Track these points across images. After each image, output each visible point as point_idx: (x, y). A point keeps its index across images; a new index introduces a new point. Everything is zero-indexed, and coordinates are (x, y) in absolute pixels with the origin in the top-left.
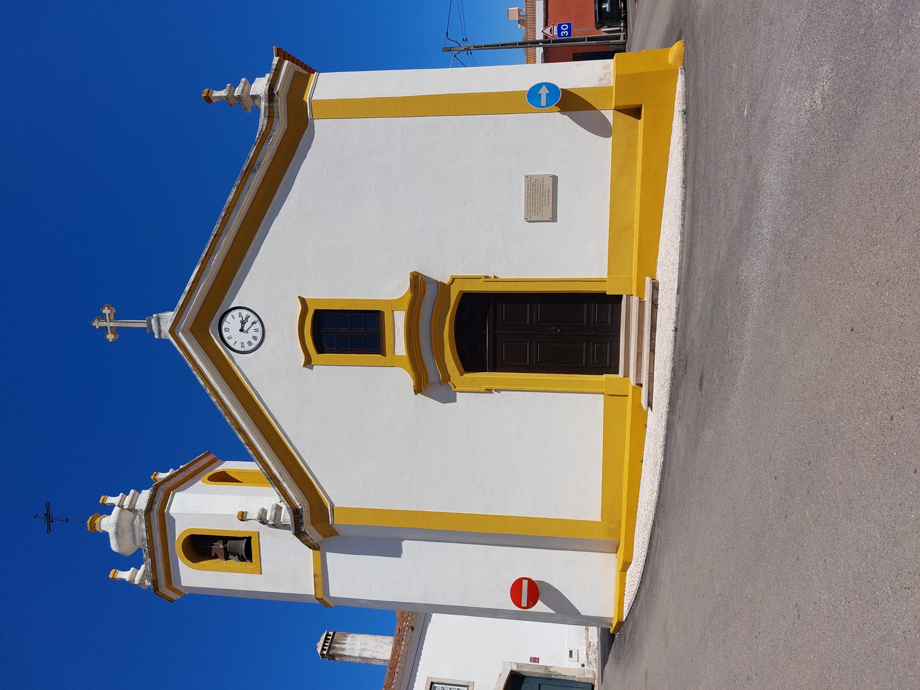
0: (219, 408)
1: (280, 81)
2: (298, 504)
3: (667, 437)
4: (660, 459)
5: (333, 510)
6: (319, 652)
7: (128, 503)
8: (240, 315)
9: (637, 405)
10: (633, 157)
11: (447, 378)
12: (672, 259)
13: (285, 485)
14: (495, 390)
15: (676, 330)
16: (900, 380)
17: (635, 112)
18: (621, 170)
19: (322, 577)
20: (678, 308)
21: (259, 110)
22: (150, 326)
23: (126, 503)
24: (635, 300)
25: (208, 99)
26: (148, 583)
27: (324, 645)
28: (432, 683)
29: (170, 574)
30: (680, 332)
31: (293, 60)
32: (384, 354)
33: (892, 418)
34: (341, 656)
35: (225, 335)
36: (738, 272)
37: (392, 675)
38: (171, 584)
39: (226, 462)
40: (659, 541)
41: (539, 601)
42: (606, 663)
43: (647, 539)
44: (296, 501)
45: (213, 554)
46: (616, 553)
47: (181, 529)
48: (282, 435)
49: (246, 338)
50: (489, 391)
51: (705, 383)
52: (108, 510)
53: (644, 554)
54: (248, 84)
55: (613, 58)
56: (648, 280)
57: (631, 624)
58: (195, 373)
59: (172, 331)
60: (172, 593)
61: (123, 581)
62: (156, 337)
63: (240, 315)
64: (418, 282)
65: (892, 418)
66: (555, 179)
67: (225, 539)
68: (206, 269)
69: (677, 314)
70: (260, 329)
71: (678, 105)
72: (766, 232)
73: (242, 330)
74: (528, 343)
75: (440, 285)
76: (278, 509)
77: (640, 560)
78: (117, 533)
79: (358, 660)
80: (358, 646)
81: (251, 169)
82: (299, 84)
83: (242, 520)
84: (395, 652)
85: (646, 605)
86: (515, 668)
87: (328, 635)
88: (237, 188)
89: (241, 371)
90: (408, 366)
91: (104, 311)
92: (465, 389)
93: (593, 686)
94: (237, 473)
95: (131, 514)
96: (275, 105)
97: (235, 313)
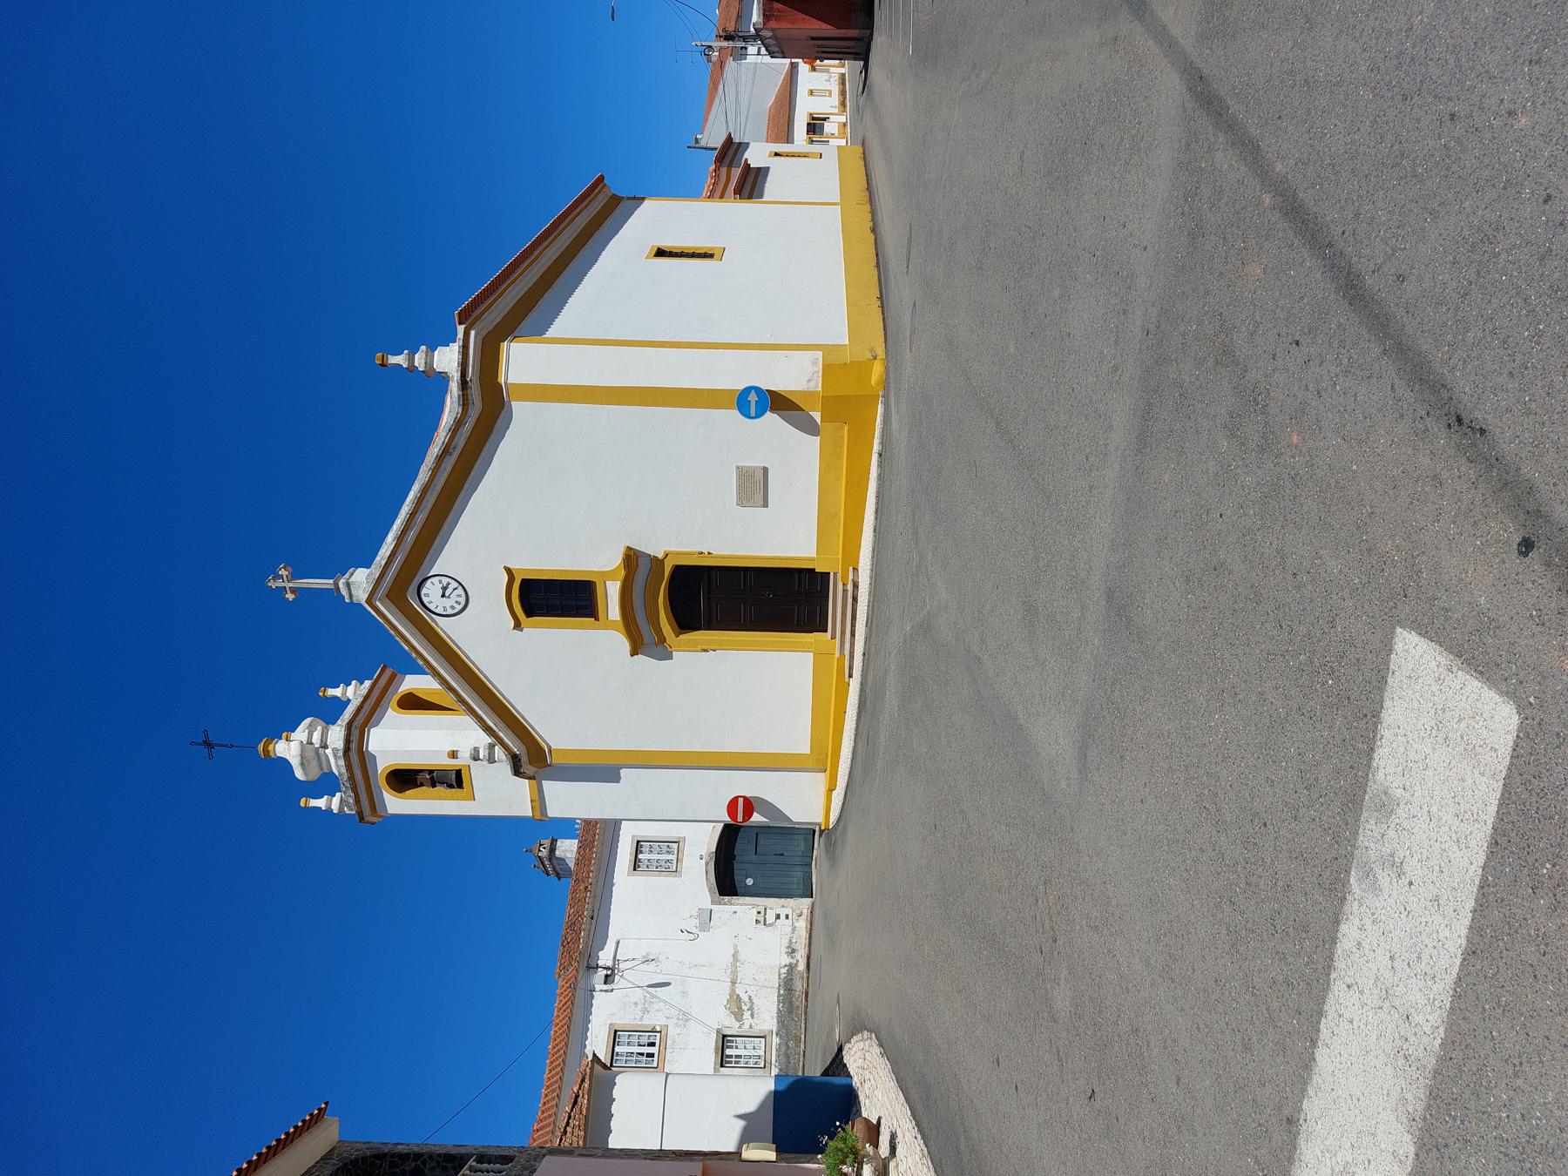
1: (471, 362)
2: (515, 750)
5: (550, 751)
8: (440, 582)
11: (662, 640)
13: (501, 734)
19: (539, 800)
22: (336, 584)
28: (638, 842)
29: (375, 804)
32: (597, 619)
35: (425, 600)
41: (755, 813)
47: (383, 765)
48: (501, 697)
49: (447, 603)
58: (397, 639)
63: (440, 582)
64: (632, 558)
66: (765, 470)
73: (443, 596)
78: (302, 764)
89: (445, 633)
90: (623, 630)
94: (426, 693)
96: (469, 392)
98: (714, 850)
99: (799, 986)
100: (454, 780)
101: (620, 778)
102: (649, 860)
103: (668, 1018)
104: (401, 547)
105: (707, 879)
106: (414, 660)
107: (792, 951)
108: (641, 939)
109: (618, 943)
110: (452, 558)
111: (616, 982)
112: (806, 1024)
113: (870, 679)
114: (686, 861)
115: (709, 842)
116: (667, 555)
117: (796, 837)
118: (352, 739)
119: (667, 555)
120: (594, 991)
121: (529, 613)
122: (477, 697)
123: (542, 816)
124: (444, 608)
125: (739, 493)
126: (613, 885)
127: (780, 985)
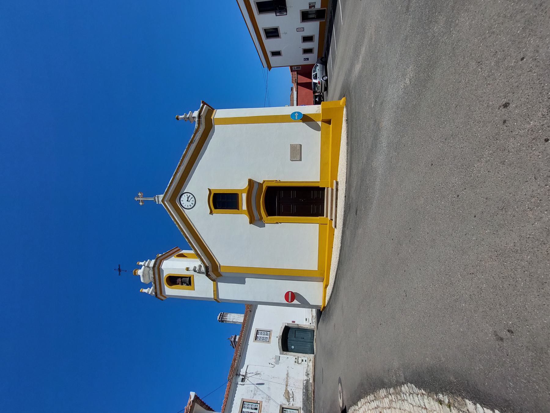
0: (179, 229)
2: (207, 264)
3: (342, 237)
4: (340, 245)
5: (220, 266)
6: (218, 320)
7: (147, 264)
8: (187, 195)
9: (331, 226)
10: (329, 134)
11: (261, 218)
12: (343, 172)
14: (279, 223)
15: (345, 197)
16: (462, 177)
17: (329, 122)
18: (324, 143)
19: (216, 291)
20: (346, 189)
21: (195, 122)
22: (155, 199)
23: (146, 265)
24: (330, 189)
25: (177, 119)
26: (154, 294)
27: (220, 317)
28: (257, 330)
30: (347, 197)
31: (207, 104)
32: (238, 209)
33: (458, 196)
34: (226, 321)
35: (182, 202)
36: (371, 165)
37: (243, 328)
38: (162, 294)
39: (183, 250)
40: (339, 275)
41: (295, 300)
42: (319, 322)
43: (335, 275)
44: (206, 263)
45: (177, 283)
46: (323, 282)
50: (277, 223)
51: (358, 212)
52: (140, 267)
53: (333, 281)
54: (192, 113)
55: (320, 104)
56: (334, 181)
57: (328, 307)
58: (170, 216)
59: (163, 201)
60: (162, 297)
61: (145, 293)
62: (157, 203)
63: (187, 195)
64: (251, 182)
65: (458, 196)
66: (301, 145)
67: (182, 278)
68: (175, 178)
69: (346, 191)
70: (194, 200)
71: (344, 118)
72: (384, 144)
73: (188, 201)
74: (291, 205)
75: (259, 184)
76: (200, 266)
77: (332, 283)
78: (143, 276)
79: (232, 322)
80: (232, 318)
81: (192, 142)
82: (210, 111)
83: (187, 270)
84: (245, 320)
85: (334, 300)
86: (287, 325)
87: (221, 314)
88: (187, 149)
91: (139, 194)
92: (268, 222)
93: (314, 331)
95: (148, 269)
97: (185, 195)
98: (281, 335)
99: (311, 389)
100: (187, 281)
101: (245, 282)
102: (260, 337)
103: (263, 398)
104: (175, 180)
105: (279, 345)
106: (175, 225)
107: (308, 375)
108: (255, 366)
109: (248, 366)
110: (191, 187)
111: (245, 381)
112: (314, 405)
113: (354, 171)
114: (272, 338)
115: (280, 332)
116: (264, 181)
117: (308, 332)
118: (157, 263)
119: (264, 181)
120: (238, 384)
121: (215, 208)
122: (196, 243)
123: (217, 298)
124: (188, 206)
125: (291, 155)
126: (248, 345)
127: (303, 388)
